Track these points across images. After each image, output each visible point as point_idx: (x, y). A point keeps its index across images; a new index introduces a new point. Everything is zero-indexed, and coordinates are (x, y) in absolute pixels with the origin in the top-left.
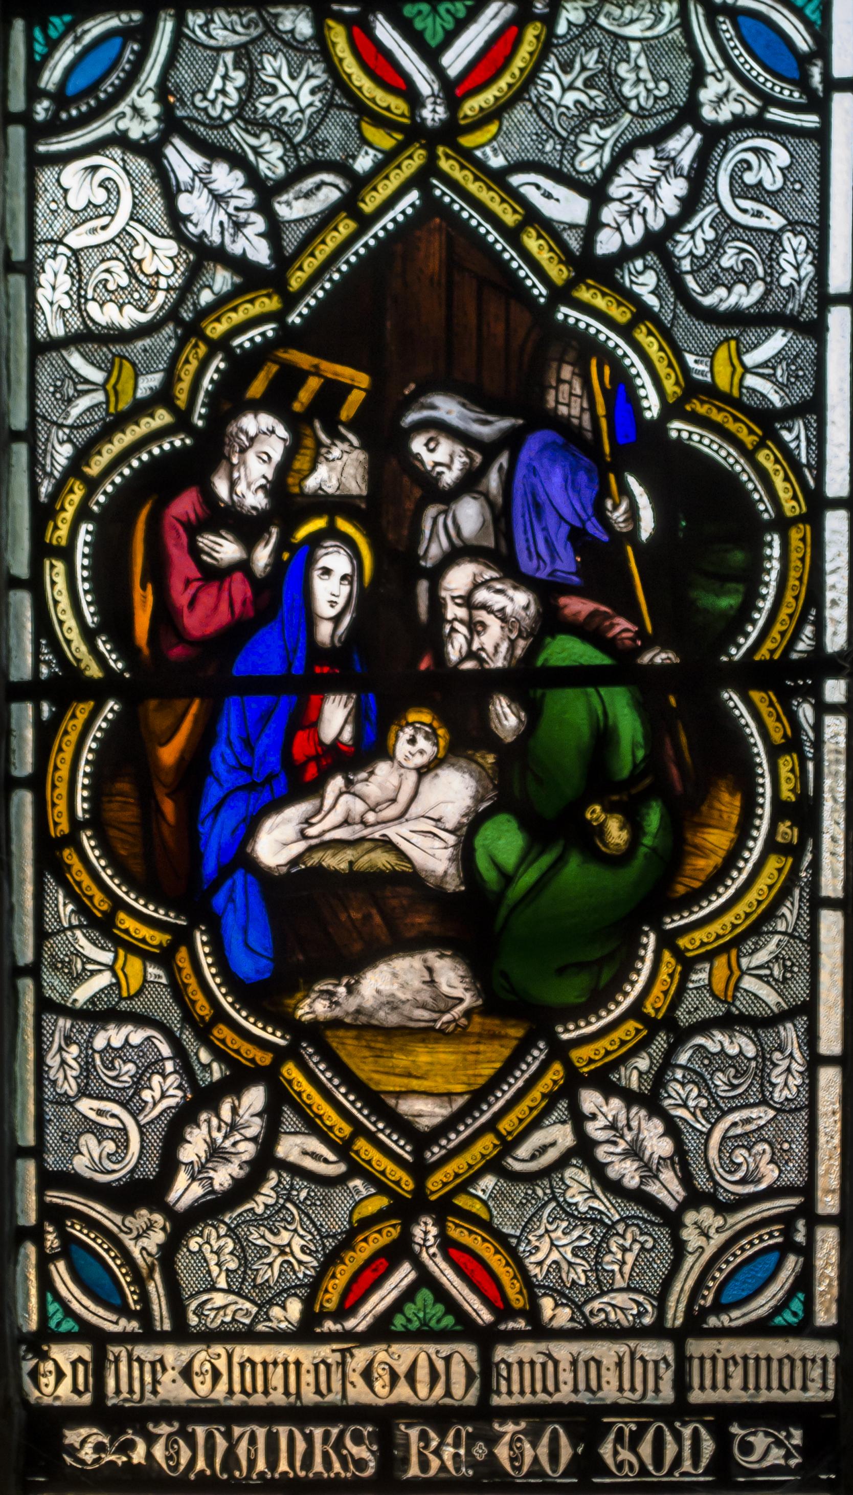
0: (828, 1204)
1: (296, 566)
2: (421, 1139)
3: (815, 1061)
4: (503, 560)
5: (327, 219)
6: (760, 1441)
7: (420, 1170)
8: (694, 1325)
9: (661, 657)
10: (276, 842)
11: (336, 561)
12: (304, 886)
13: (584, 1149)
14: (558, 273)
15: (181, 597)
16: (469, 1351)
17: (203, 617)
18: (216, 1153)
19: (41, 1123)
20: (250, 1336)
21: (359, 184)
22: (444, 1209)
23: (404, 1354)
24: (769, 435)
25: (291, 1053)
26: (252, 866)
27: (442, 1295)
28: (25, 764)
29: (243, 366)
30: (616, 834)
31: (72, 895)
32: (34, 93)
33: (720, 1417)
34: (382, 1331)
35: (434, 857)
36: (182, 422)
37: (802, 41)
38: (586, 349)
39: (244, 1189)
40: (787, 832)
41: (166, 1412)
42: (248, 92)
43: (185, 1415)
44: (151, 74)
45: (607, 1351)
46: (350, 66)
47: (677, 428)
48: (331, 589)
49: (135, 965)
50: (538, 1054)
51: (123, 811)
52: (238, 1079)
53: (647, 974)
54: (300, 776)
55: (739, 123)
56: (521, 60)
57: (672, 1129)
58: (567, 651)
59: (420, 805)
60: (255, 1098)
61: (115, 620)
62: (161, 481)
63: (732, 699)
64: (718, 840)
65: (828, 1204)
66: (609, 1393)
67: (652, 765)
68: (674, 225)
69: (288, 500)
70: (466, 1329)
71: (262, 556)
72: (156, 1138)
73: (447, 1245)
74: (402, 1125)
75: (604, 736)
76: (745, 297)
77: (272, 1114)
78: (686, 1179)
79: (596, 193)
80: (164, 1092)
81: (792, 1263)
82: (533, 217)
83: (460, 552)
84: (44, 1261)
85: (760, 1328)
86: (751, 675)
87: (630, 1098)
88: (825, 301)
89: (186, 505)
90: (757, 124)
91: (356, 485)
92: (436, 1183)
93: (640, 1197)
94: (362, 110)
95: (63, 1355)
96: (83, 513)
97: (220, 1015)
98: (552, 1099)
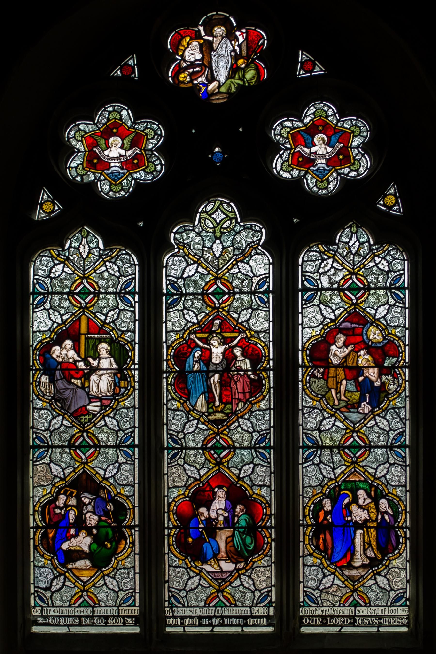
0: (137, 591)
1: (67, 514)
2: (84, 583)
3: (135, 573)
4: (94, 513)
5: (71, 472)
6: (129, 620)
7: (84, 586)
8: (120, 605)
9: (114, 525)
10: (65, 546)
11: (72, 512)
12: (69, 552)
13: (105, 584)
14: (101, 479)
15: (52, 516)
16: (91, 609)
17: (55, 520)
18: (57, 584)
19: (34, 580)
20: (62, 607)
21: (75, 469)
22: (87, 591)
23: (82, 609)
24: (128, 499)
25: (67, 572)
26: (62, 549)
27: (87, 602)
28: (32, 536)
29: (60, 490)
30: (109, 545)
31: (38, 552)
32: (33, 458)
33: (124, 617)
34: (79, 606)
35: (86, 549)
36: (52, 496)
37: (131, 454)
38: (104, 488)
39: (61, 589)
40: (131, 545)
41: (51, 616)
42: (61, 458)
43: (53, 617)
44: (48, 456)
45: (109, 609)
46: (74, 455)
47: (116, 498)
48: (72, 516)
49: (46, 561)
50: (99, 572)
51: (44, 542)
52: (60, 575)
53: (114, 563)
54: (68, 539)
55: (123, 463)
56: (344, 439)
57: (117, 581)
58: (103, 524)
59: (83, 542)
60: (62, 577)
61: (44, 519)
62: (50, 503)
63: (123, 529)
64: (122, 546)
65: (137, 591)
66: (109, 614)
67: (114, 537)
68: (115, 474)
69: (66, 505)
70: (90, 606)
71: (63, 512)
72: (49, 582)
73: (88, 596)
74: (82, 581)
75: (107, 534)
76: (125, 483)
77: (65, 579)
78: (119, 587)
79: (105, 470)
80: (51, 576)
81: (133, 598)
82: (97, 473)
83: (88, 512)
84: (35, 597)
85: (129, 606)
86: (125, 527)
87: (111, 578)
88: (135, 483)
89: (53, 505)
90: (126, 463)
91: (75, 504)
92: (86, 588)
93: (113, 590)
94: (75, 460)
95: (37, 609)
96: (40, 506)
97: (58, 567)
98: (101, 578)
